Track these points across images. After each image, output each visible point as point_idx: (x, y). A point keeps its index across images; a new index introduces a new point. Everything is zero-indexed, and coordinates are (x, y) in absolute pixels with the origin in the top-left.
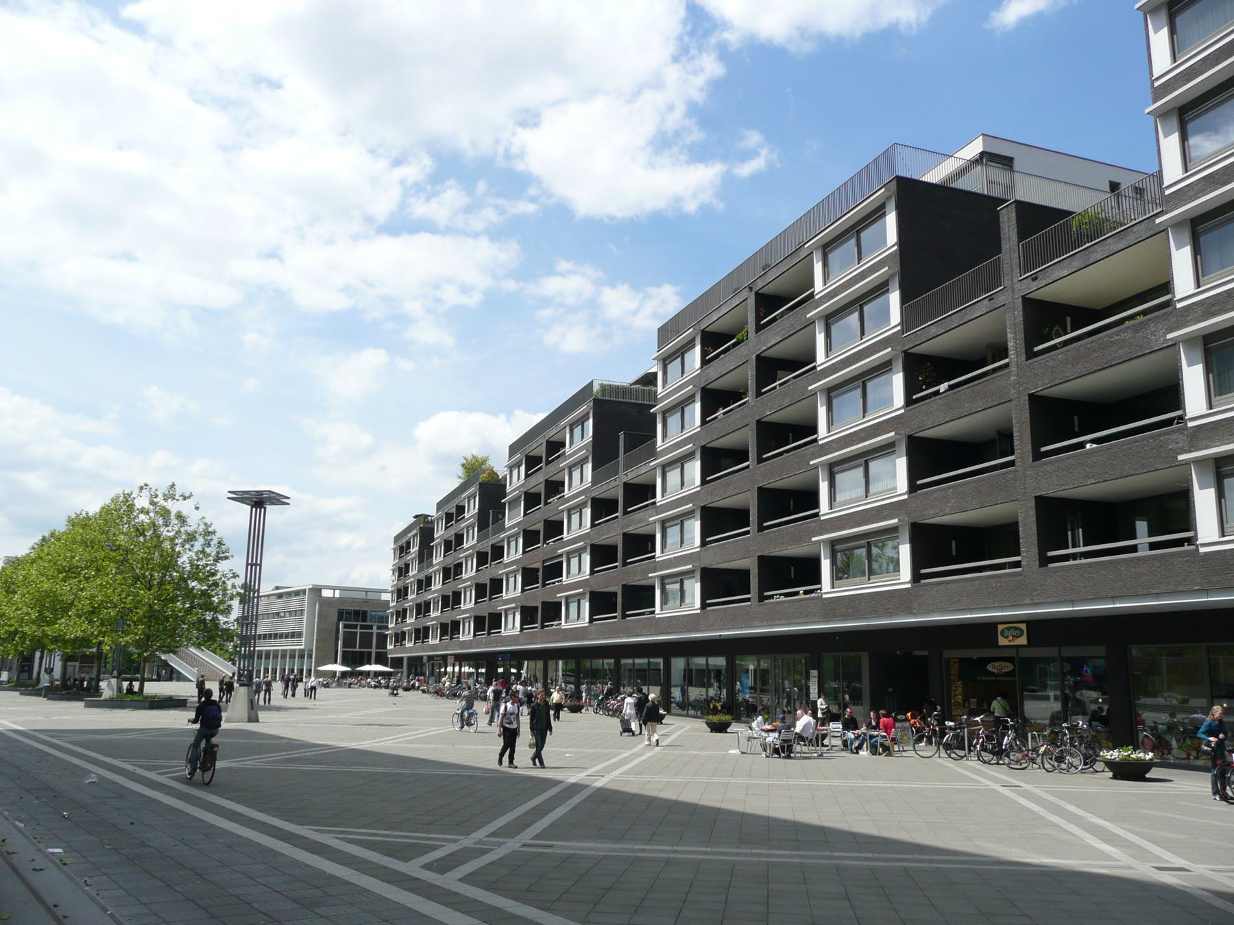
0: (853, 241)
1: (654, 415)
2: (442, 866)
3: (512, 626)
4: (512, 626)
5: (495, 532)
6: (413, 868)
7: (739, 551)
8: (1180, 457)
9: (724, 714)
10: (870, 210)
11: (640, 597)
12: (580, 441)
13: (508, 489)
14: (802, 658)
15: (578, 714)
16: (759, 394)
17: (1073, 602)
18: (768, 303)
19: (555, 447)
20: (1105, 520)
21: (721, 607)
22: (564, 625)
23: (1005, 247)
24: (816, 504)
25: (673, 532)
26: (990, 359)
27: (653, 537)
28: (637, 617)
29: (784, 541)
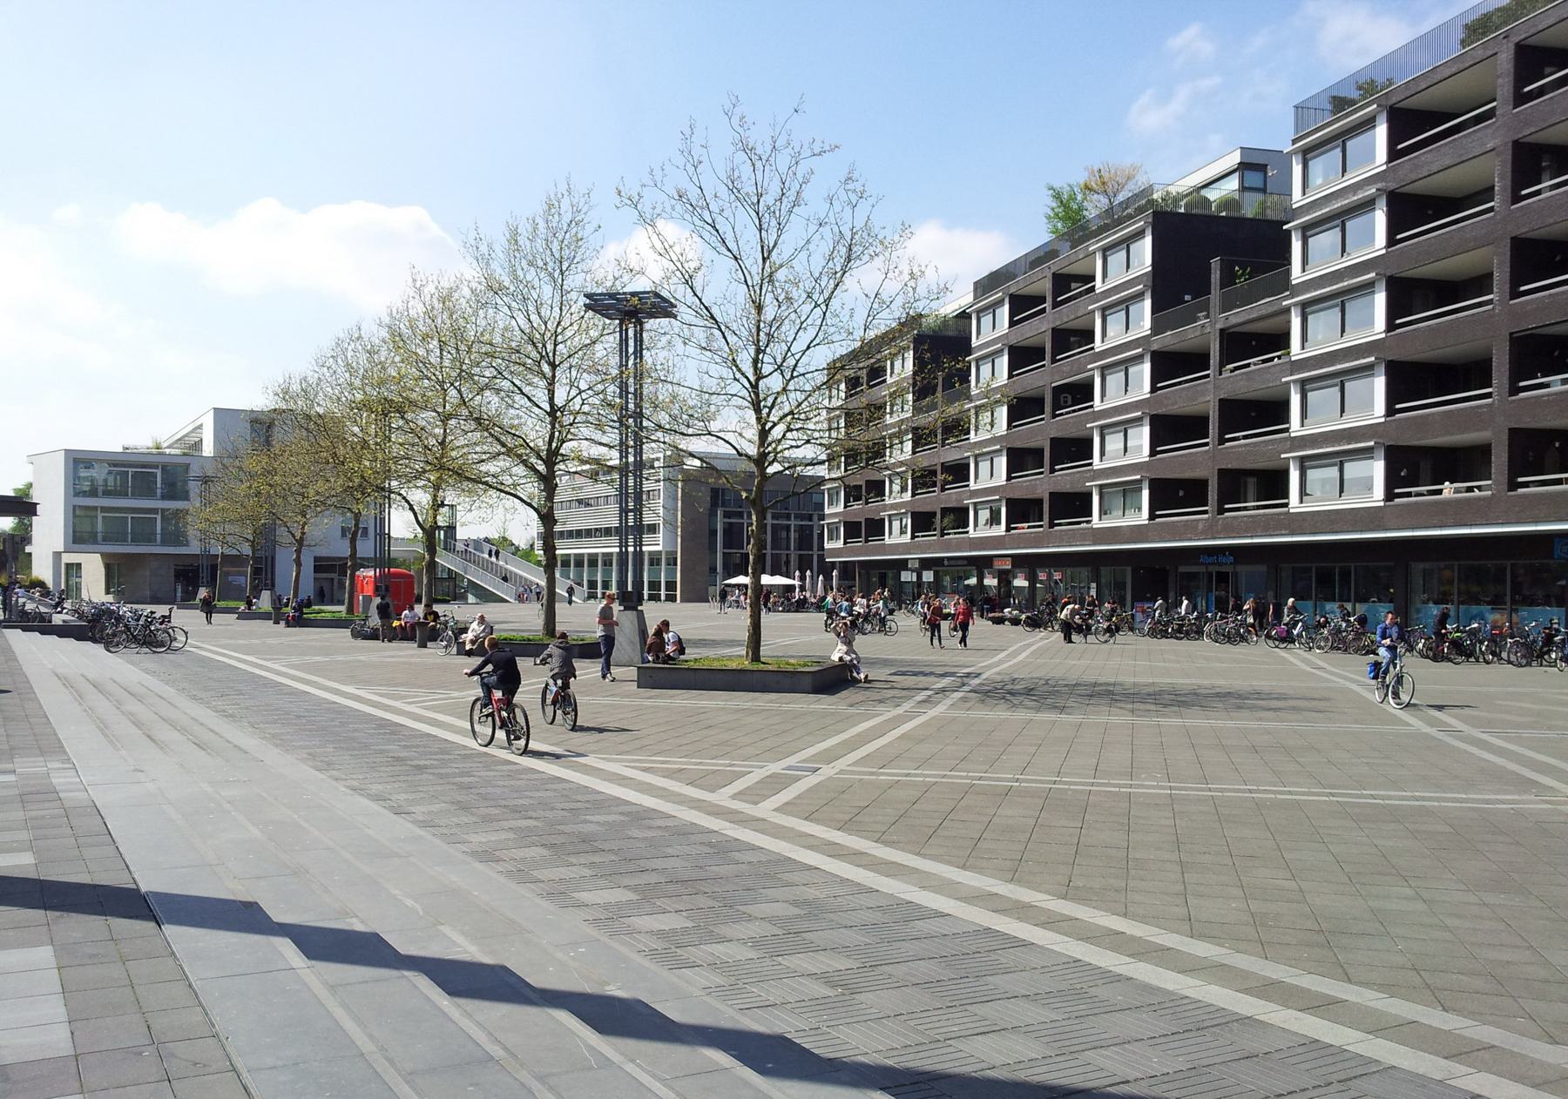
0: (1337, 153)
1: (1289, 232)
2: (755, 794)
3: (897, 536)
4: (897, 536)
5: (950, 401)
6: (723, 797)
7: (1039, 483)
9: (1266, 623)
11: (1074, 505)
12: (903, 368)
13: (975, 343)
16: (1054, 361)
18: (1062, 282)
19: (876, 373)
20: (1234, 485)
22: (888, 541)
27: (1091, 441)
28: (1251, 509)
29: (1066, 478)
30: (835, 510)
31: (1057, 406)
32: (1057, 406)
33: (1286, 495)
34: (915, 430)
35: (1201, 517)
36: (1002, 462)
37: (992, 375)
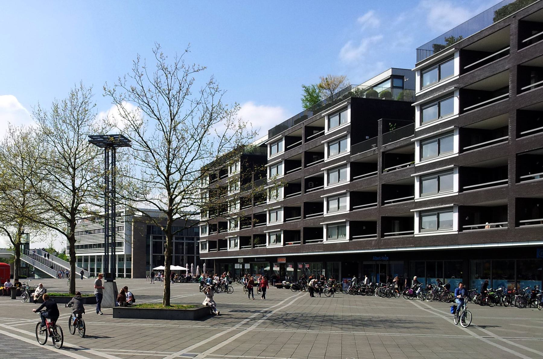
0: (437, 69)
1: (414, 107)
3: (233, 247)
4: (233, 247)
8: (411, 211)
10: (446, 56)
11: (315, 233)
12: (236, 170)
14: (320, 264)
15: (281, 289)
17: (448, 245)
18: (309, 130)
19: (224, 172)
21: (361, 239)
22: (229, 250)
23: (379, 135)
24: (413, 193)
25: (273, 215)
26: (313, 186)
28: (310, 243)
30: (204, 235)
31: (307, 187)
32: (307, 187)
33: (413, 229)
34: (241, 199)
35: (373, 238)
36: (282, 213)
37: (277, 173)
